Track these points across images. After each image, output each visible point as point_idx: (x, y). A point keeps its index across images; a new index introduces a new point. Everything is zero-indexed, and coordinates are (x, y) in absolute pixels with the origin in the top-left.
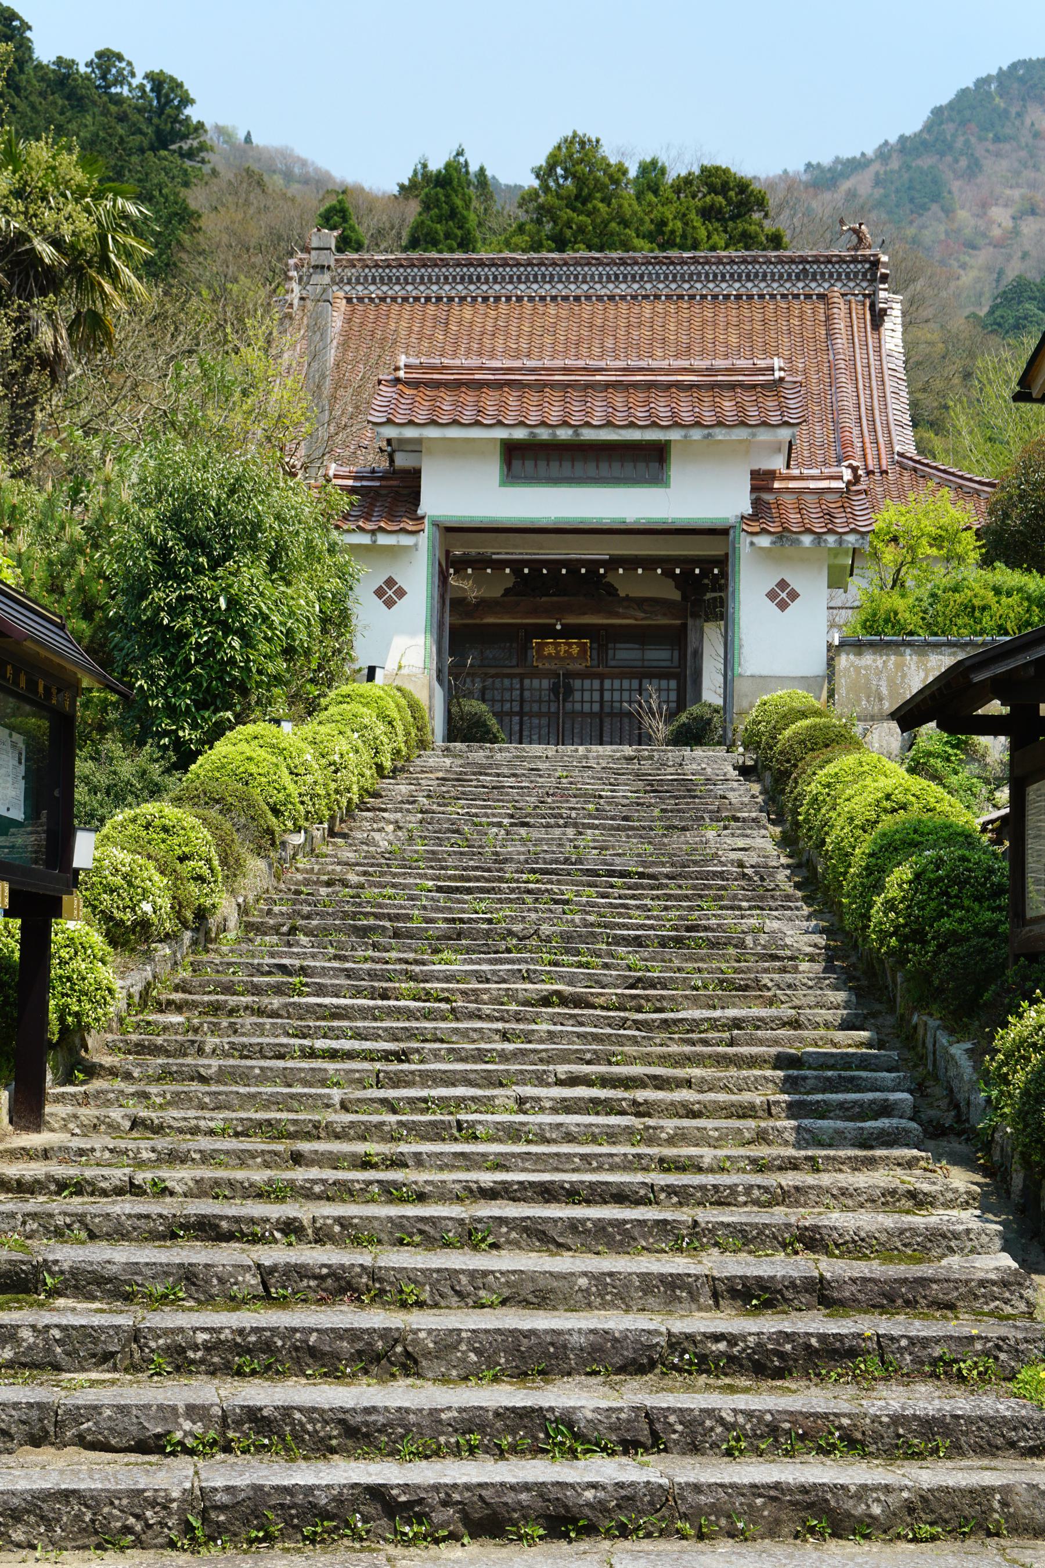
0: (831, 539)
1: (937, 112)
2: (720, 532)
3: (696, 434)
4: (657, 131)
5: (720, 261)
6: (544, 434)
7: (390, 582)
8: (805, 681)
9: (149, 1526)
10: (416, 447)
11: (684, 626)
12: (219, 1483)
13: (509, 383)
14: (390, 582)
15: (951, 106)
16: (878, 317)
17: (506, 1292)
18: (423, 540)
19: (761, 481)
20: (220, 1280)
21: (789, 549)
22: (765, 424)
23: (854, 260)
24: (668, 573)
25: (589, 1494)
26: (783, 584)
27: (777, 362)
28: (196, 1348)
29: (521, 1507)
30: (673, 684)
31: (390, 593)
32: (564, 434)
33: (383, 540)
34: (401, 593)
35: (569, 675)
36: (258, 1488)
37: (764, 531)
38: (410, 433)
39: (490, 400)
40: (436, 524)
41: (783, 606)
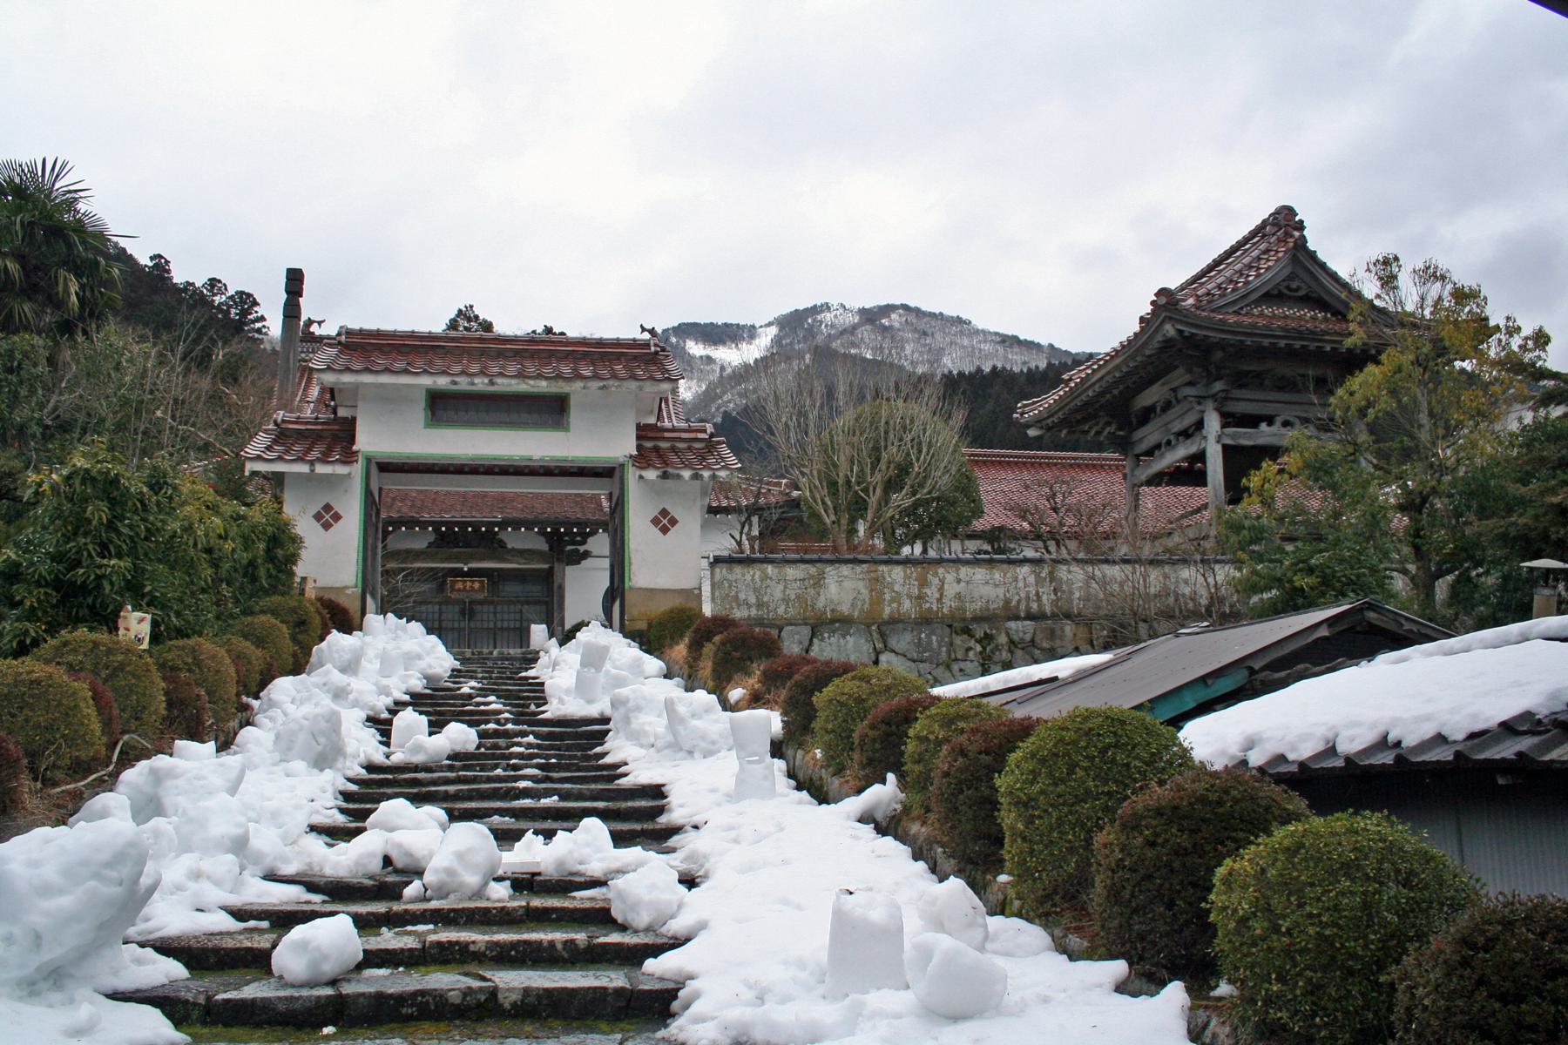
2: (606, 472)
7: (328, 508)
11: (551, 568)
14: (328, 508)
18: (357, 469)
21: (669, 483)
24: (542, 533)
26: (664, 513)
34: (337, 517)
40: (369, 460)
41: (665, 530)
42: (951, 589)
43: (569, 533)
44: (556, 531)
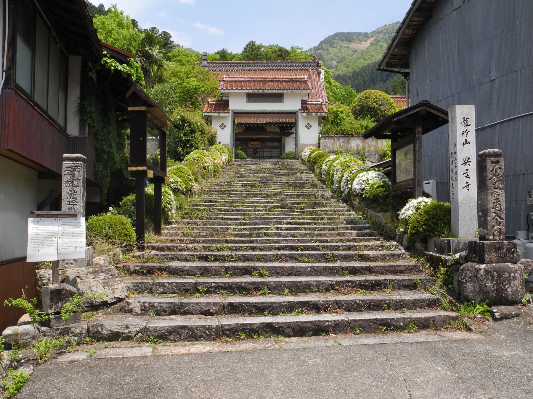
0: (319, 114)
1: (321, 42)
2: (293, 114)
3: (290, 91)
4: (266, 40)
5: (286, 63)
6: (256, 91)
7: (223, 124)
8: (313, 145)
9: (207, 335)
10: (228, 95)
12: (226, 323)
13: (248, 81)
14: (223, 124)
15: (323, 41)
16: (319, 74)
17: (290, 272)
19: (304, 102)
20: (215, 270)
21: (310, 116)
22: (304, 89)
23: (314, 63)
25: (327, 323)
26: (308, 124)
27: (306, 77)
28: (212, 288)
29: (309, 328)
30: (279, 150)
31: (223, 126)
32: (261, 91)
33: (221, 115)
34: (225, 126)
35: (257, 148)
36: (237, 324)
37: (304, 112)
38: (227, 91)
39: (244, 84)
40: (232, 111)
41: (308, 129)
42: (338, 144)
43: (286, 126)
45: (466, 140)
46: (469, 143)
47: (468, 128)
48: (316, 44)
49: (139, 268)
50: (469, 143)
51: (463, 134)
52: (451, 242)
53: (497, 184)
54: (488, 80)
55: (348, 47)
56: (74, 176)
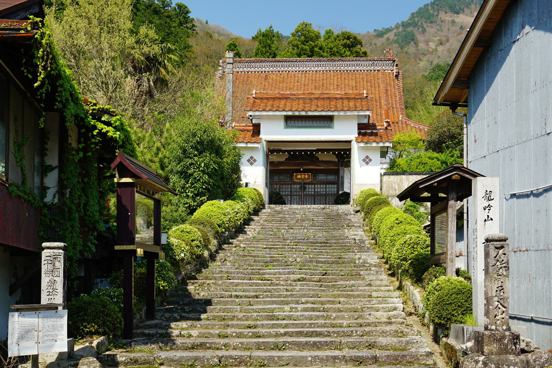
7: (252, 158)
14: (252, 158)
24: (334, 153)
26: (367, 157)
30: (336, 186)
33: (249, 145)
34: (255, 161)
35: (305, 184)
44: (339, 153)
45: (488, 216)
46: (492, 219)
47: (491, 203)
48: (406, 18)
49: (124, 358)
50: (492, 219)
51: (485, 209)
52: (465, 330)
53: (501, 271)
54: (544, 133)
55: (453, 22)
56: (54, 265)
